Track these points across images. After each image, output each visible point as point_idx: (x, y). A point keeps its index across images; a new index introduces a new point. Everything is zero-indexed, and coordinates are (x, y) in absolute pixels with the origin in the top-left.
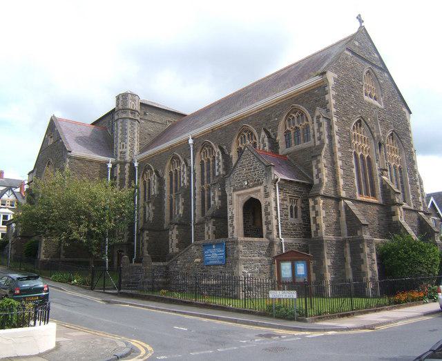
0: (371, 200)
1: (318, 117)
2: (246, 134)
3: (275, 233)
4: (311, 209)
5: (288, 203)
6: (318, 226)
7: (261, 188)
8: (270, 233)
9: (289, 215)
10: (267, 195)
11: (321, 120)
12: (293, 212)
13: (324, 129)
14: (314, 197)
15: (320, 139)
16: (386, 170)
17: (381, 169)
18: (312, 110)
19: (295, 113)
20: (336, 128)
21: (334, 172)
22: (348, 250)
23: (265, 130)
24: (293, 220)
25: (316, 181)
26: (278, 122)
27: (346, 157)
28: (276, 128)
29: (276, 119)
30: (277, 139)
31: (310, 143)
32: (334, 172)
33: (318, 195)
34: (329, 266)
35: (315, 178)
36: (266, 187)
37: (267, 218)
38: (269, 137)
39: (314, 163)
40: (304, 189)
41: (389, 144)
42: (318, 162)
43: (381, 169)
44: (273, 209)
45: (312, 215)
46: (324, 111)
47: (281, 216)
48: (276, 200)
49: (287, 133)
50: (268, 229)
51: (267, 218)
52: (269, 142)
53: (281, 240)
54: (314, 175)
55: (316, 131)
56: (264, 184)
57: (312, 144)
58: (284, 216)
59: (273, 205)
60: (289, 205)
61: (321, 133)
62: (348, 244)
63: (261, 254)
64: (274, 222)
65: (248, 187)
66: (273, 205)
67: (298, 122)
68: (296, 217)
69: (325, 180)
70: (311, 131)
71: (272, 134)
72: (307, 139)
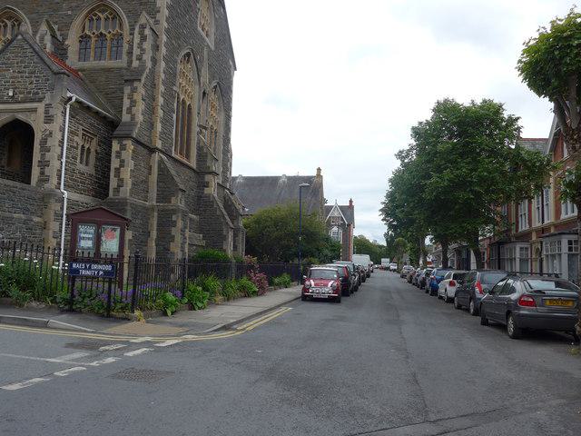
0: (185, 161)
1: (143, 27)
2: (9, 23)
3: (54, 181)
4: (113, 155)
5: (78, 140)
6: (121, 183)
7: (41, 107)
8: (44, 179)
9: (79, 158)
10: (49, 119)
11: (147, 32)
12: (85, 152)
13: (147, 45)
14: (121, 138)
15: (139, 58)
16: (205, 128)
17: (200, 126)
18: (134, 16)
19: (103, 12)
20: (163, 50)
21: (151, 110)
22: (155, 222)
23: (48, 22)
24: (82, 167)
25: (126, 118)
26: (71, 19)
27: (170, 95)
28: (68, 26)
29: (70, 13)
30: (66, 43)
31: (122, 62)
32: (151, 110)
33: (128, 137)
34: (130, 240)
35: (124, 112)
36: (48, 106)
37: (43, 155)
38: (53, 36)
39: (127, 90)
40: (108, 128)
41: (212, 96)
42: (134, 90)
43: (200, 126)
44: (57, 143)
45: (115, 163)
46: (152, 21)
47: (67, 157)
48: (62, 130)
49: (84, 39)
50: (42, 173)
51: (43, 155)
52: (53, 43)
53: (63, 193)
54: (124, 108)
55: (135, 45)
56: (47, 101)
57: (125, 65)
58: (71, 158)
59: (58, 136)
60: (81, 143)
61: (143, 50)
62: (156, 214)
63: (28, 210)
64: (55, 164)
65: (13, 100)
66: (58, 136)
67: (106, 28)
68: (87, 165)
69: (140, 118)
70: (126, 47)
71: (58, 33)
72: (118, 56)
